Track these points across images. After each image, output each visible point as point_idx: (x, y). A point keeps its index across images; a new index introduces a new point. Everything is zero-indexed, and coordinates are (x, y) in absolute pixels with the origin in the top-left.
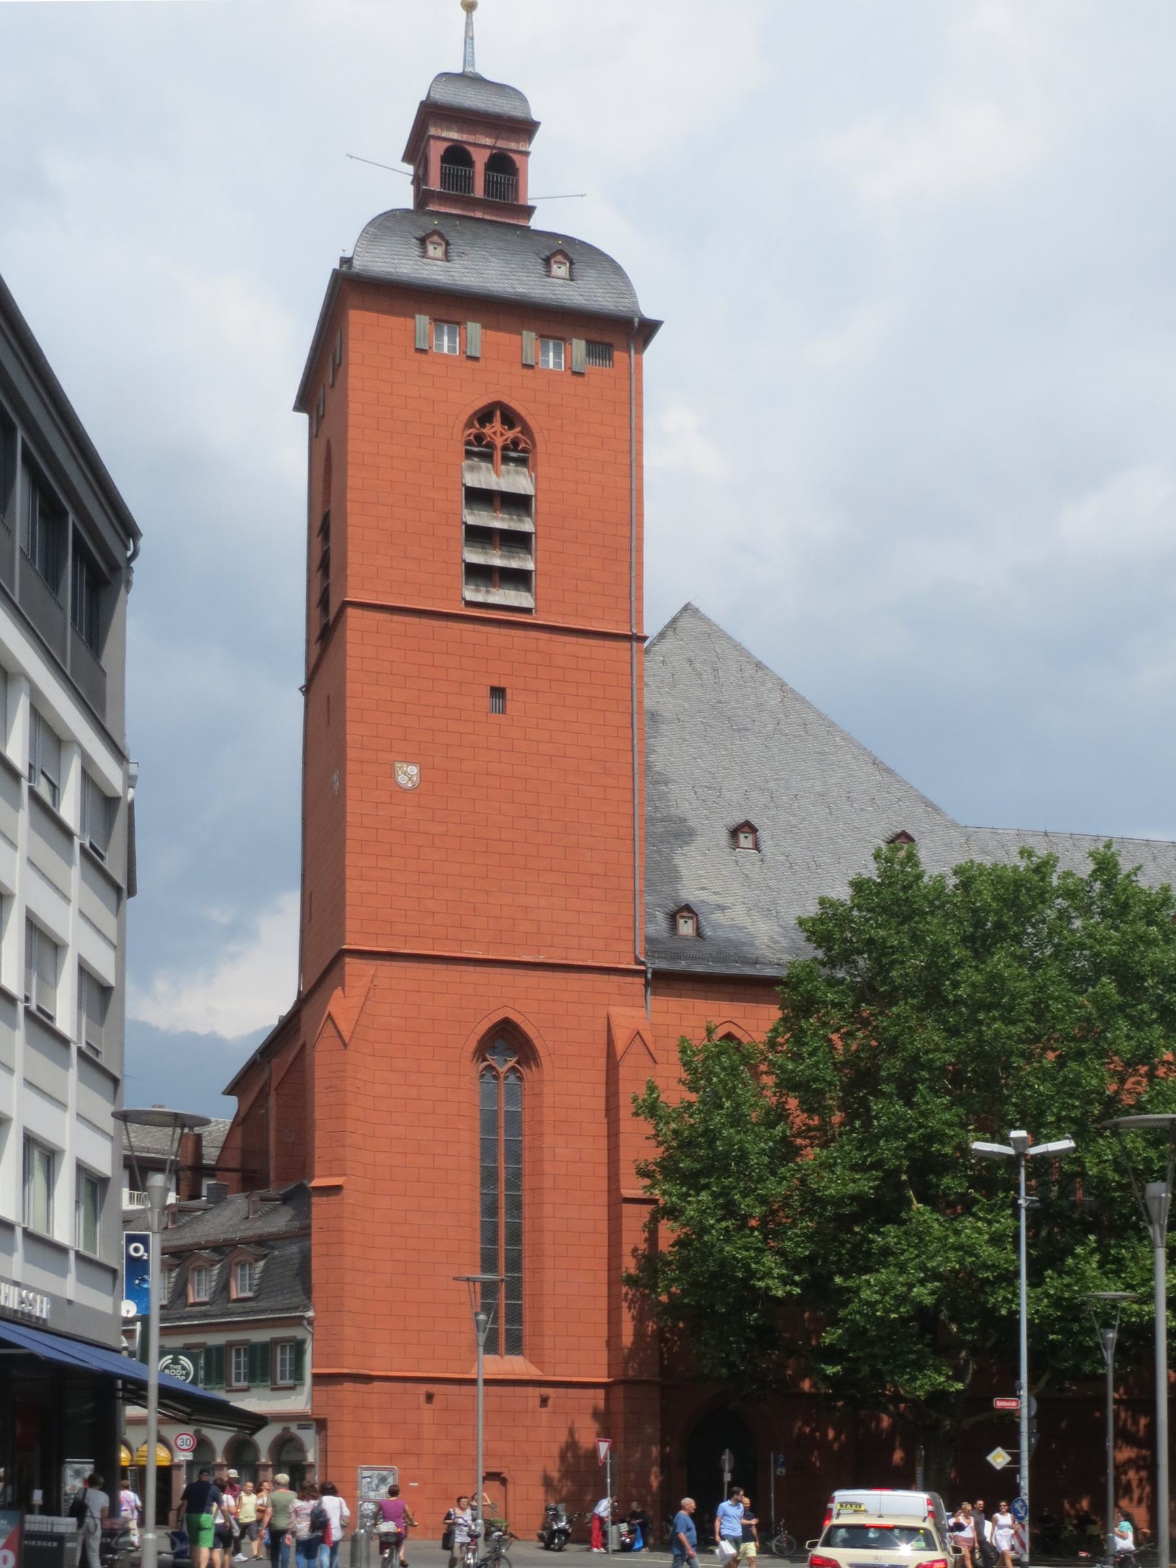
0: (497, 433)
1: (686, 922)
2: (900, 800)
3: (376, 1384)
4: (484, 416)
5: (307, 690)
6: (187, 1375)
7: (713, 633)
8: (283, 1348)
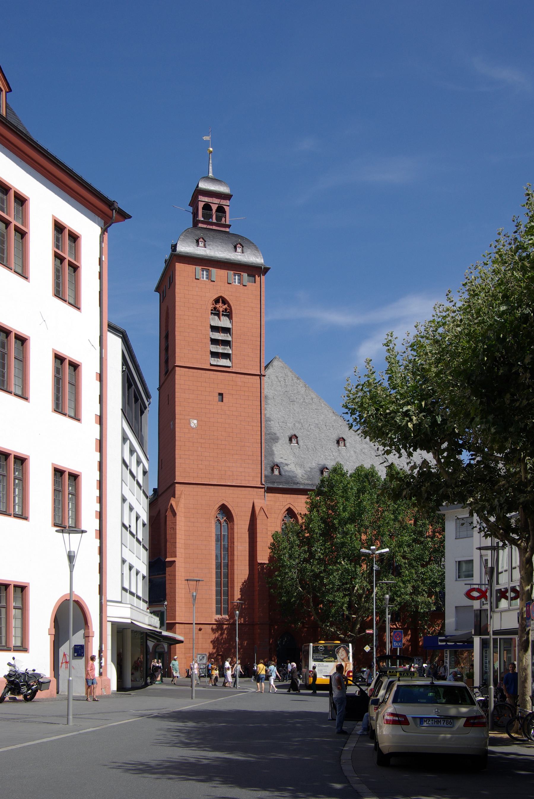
0: (221, 307)
4: (217, 301)
5: (159, 389)
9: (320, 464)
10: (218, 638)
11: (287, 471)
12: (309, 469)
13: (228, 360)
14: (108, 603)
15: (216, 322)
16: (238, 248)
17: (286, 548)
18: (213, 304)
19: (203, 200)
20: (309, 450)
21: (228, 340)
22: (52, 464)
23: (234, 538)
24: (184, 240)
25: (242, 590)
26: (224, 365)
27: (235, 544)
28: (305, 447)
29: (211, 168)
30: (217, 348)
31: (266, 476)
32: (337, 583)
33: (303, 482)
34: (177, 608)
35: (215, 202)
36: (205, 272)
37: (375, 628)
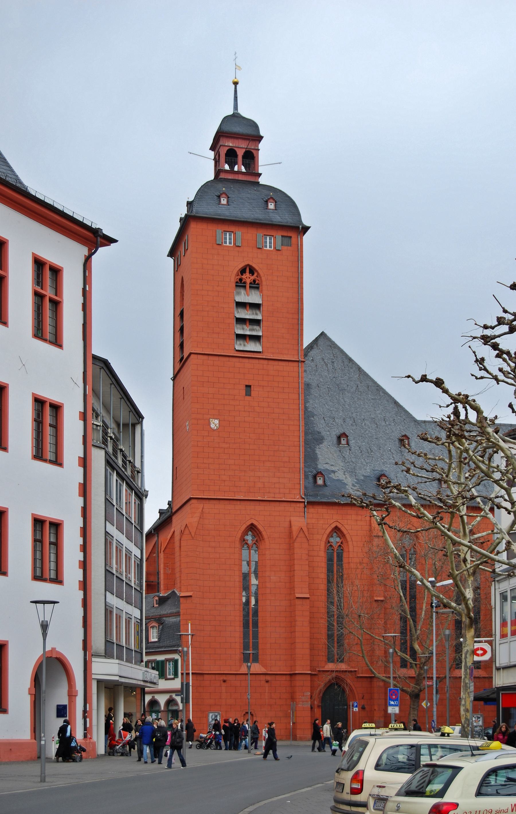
0: (248, 278)
1: (320, 479)
3: (206, 676)
4: (243, 271)
5: (174, 379)
7: (333, 345)
14: (94, 659)
15: (243, 297)
22: (32, 514)
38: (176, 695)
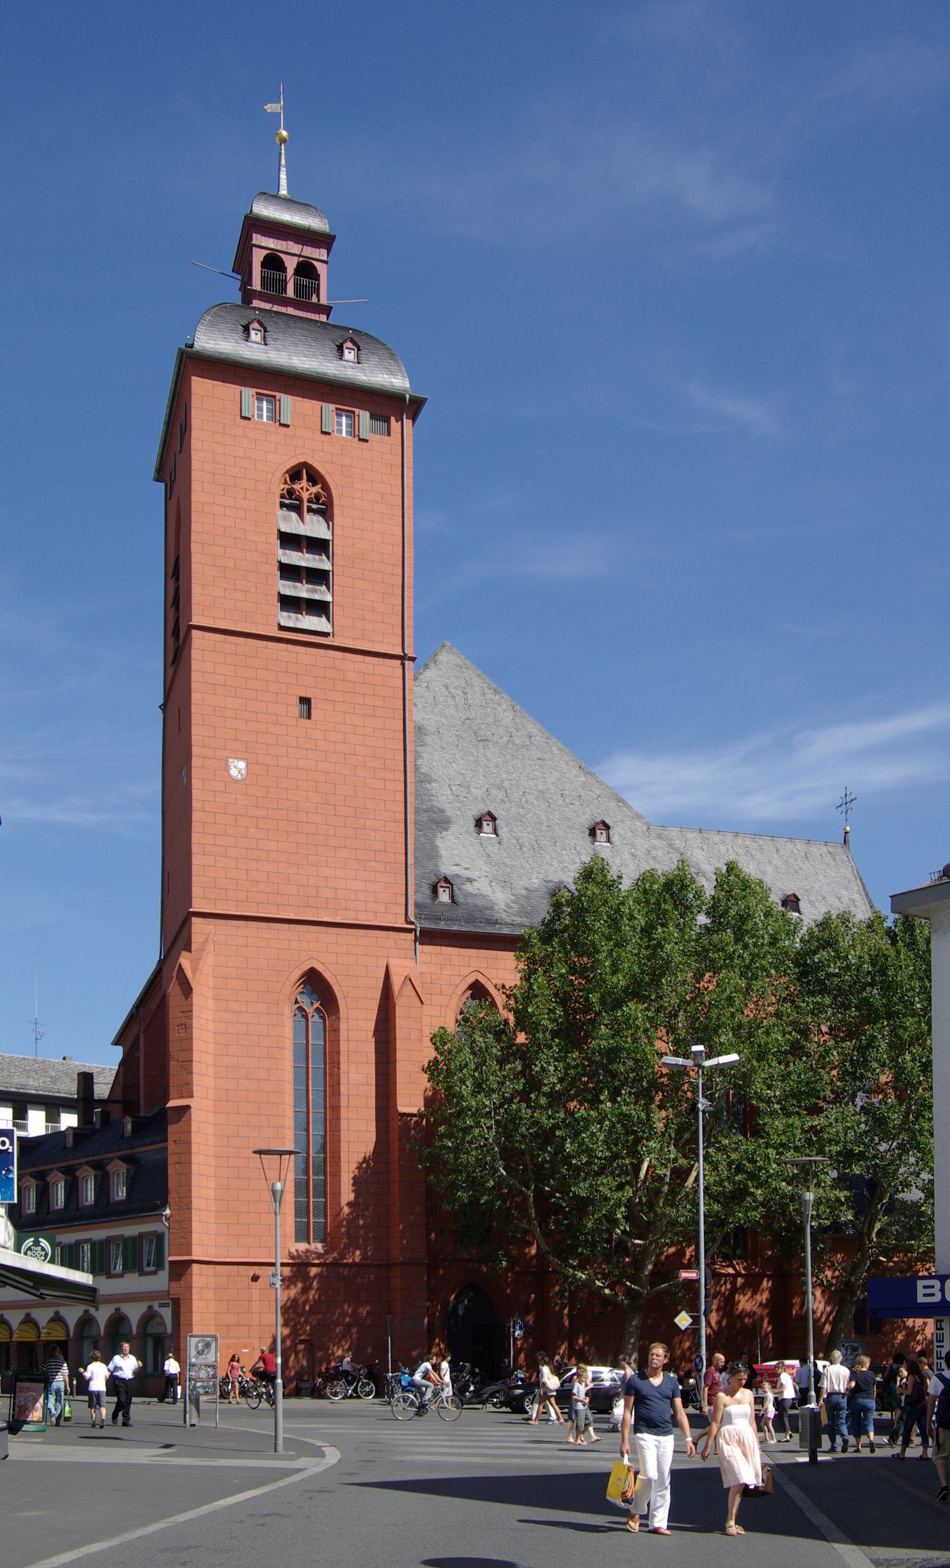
2: (599, 797)
4: (295, 474)
5: (164, 707)
6: (46, 1255)
8: (151, 1241)
9: (551, 881)
10: (295, 1301)
11: (470, 894)
12: (524, 892)
13: (324, 619)
15: (292, 524)
16: (346, 352)
17: (466, 1065)
18: (286, 483)
19: (263, 244)
20: (524, 849)
21: (323, 568)
23: (338, 1053)
24: (212, 324)
25: (356, 1181)
26: (313, 629)
27: (343, 1067)
28: (514, 841)
29: (283, 176)
30: (295, 587)
31: (417, 905)
32: (602, 1152)
33: (508, 920)
34: (195, 1225)
35: (292, 251)
36: (265, 403)
37: (703, 1266)
38: (161, 1305)
